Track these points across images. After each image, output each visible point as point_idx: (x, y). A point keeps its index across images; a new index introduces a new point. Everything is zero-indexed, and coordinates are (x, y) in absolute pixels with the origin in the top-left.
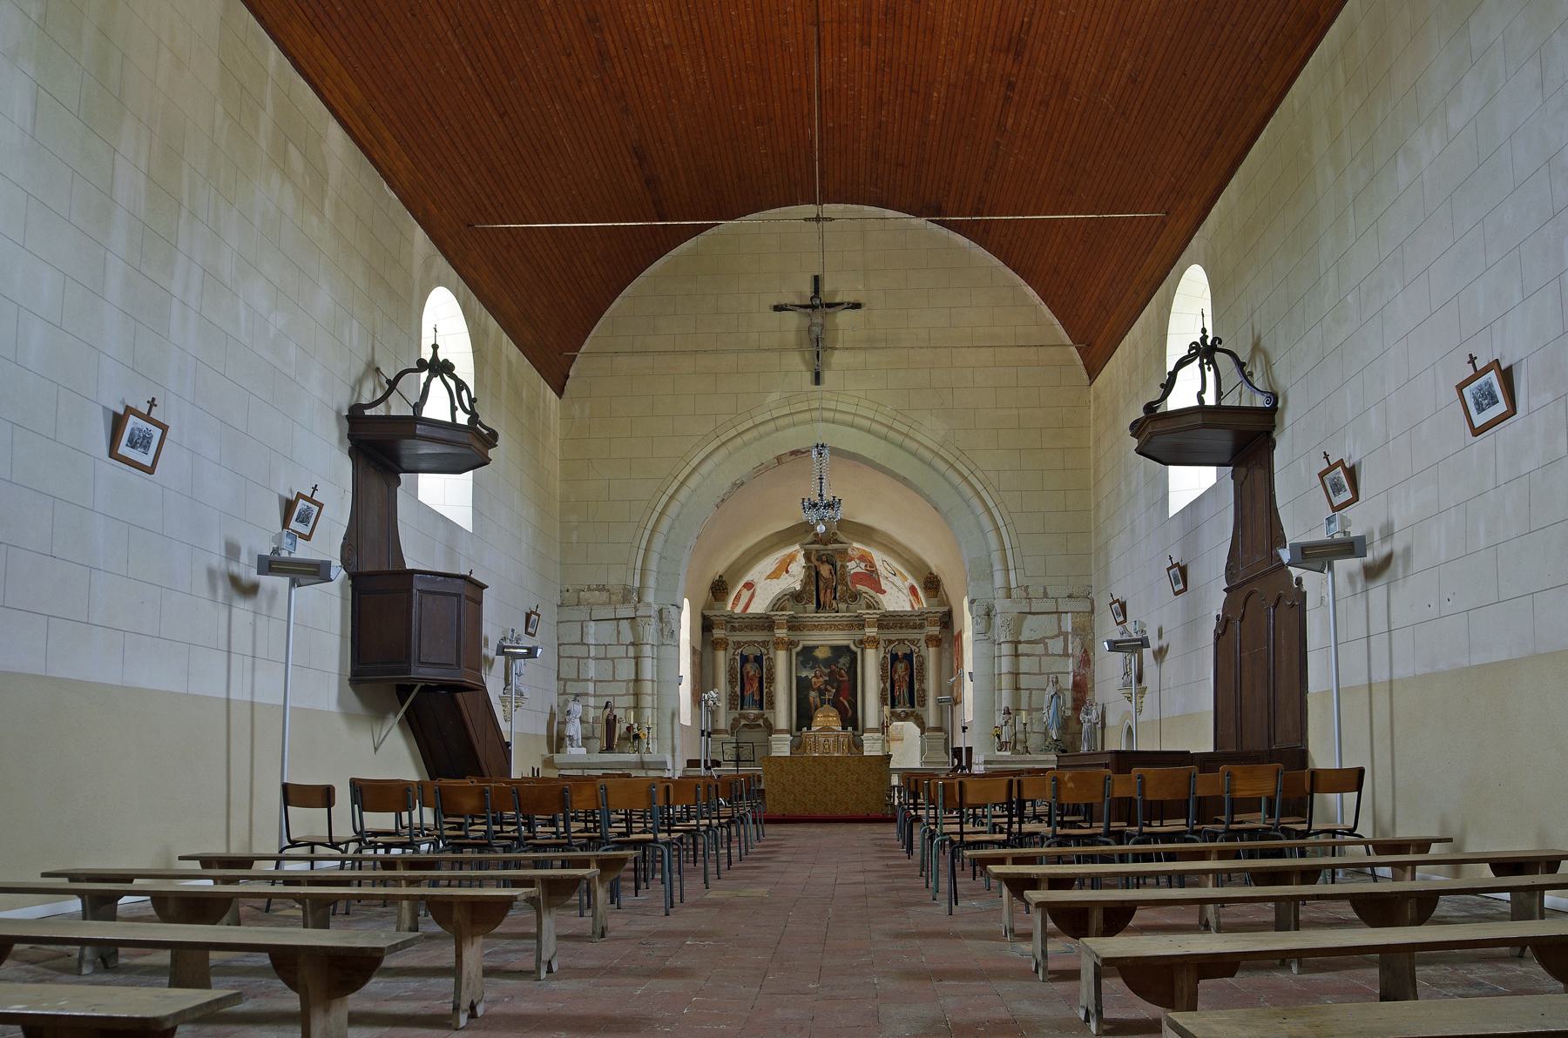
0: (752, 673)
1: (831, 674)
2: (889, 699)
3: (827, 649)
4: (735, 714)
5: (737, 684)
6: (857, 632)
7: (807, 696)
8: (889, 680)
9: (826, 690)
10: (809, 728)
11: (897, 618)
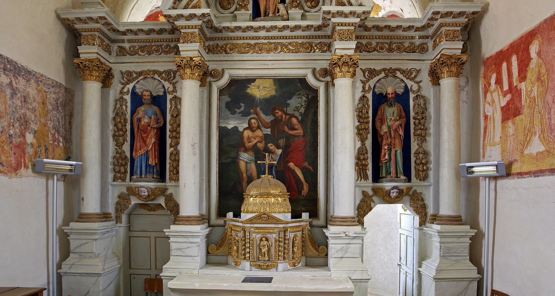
0: (145, 121)
1: (274, 124)
2: (370, 167)
3: (269, 84)
4: (121, 187)
5: (125, 140)
6: (318, 55)
7: (235, 161)
8: (370, 136)
9: (267, 150)
10: (237, 215)
11: (386, 33)
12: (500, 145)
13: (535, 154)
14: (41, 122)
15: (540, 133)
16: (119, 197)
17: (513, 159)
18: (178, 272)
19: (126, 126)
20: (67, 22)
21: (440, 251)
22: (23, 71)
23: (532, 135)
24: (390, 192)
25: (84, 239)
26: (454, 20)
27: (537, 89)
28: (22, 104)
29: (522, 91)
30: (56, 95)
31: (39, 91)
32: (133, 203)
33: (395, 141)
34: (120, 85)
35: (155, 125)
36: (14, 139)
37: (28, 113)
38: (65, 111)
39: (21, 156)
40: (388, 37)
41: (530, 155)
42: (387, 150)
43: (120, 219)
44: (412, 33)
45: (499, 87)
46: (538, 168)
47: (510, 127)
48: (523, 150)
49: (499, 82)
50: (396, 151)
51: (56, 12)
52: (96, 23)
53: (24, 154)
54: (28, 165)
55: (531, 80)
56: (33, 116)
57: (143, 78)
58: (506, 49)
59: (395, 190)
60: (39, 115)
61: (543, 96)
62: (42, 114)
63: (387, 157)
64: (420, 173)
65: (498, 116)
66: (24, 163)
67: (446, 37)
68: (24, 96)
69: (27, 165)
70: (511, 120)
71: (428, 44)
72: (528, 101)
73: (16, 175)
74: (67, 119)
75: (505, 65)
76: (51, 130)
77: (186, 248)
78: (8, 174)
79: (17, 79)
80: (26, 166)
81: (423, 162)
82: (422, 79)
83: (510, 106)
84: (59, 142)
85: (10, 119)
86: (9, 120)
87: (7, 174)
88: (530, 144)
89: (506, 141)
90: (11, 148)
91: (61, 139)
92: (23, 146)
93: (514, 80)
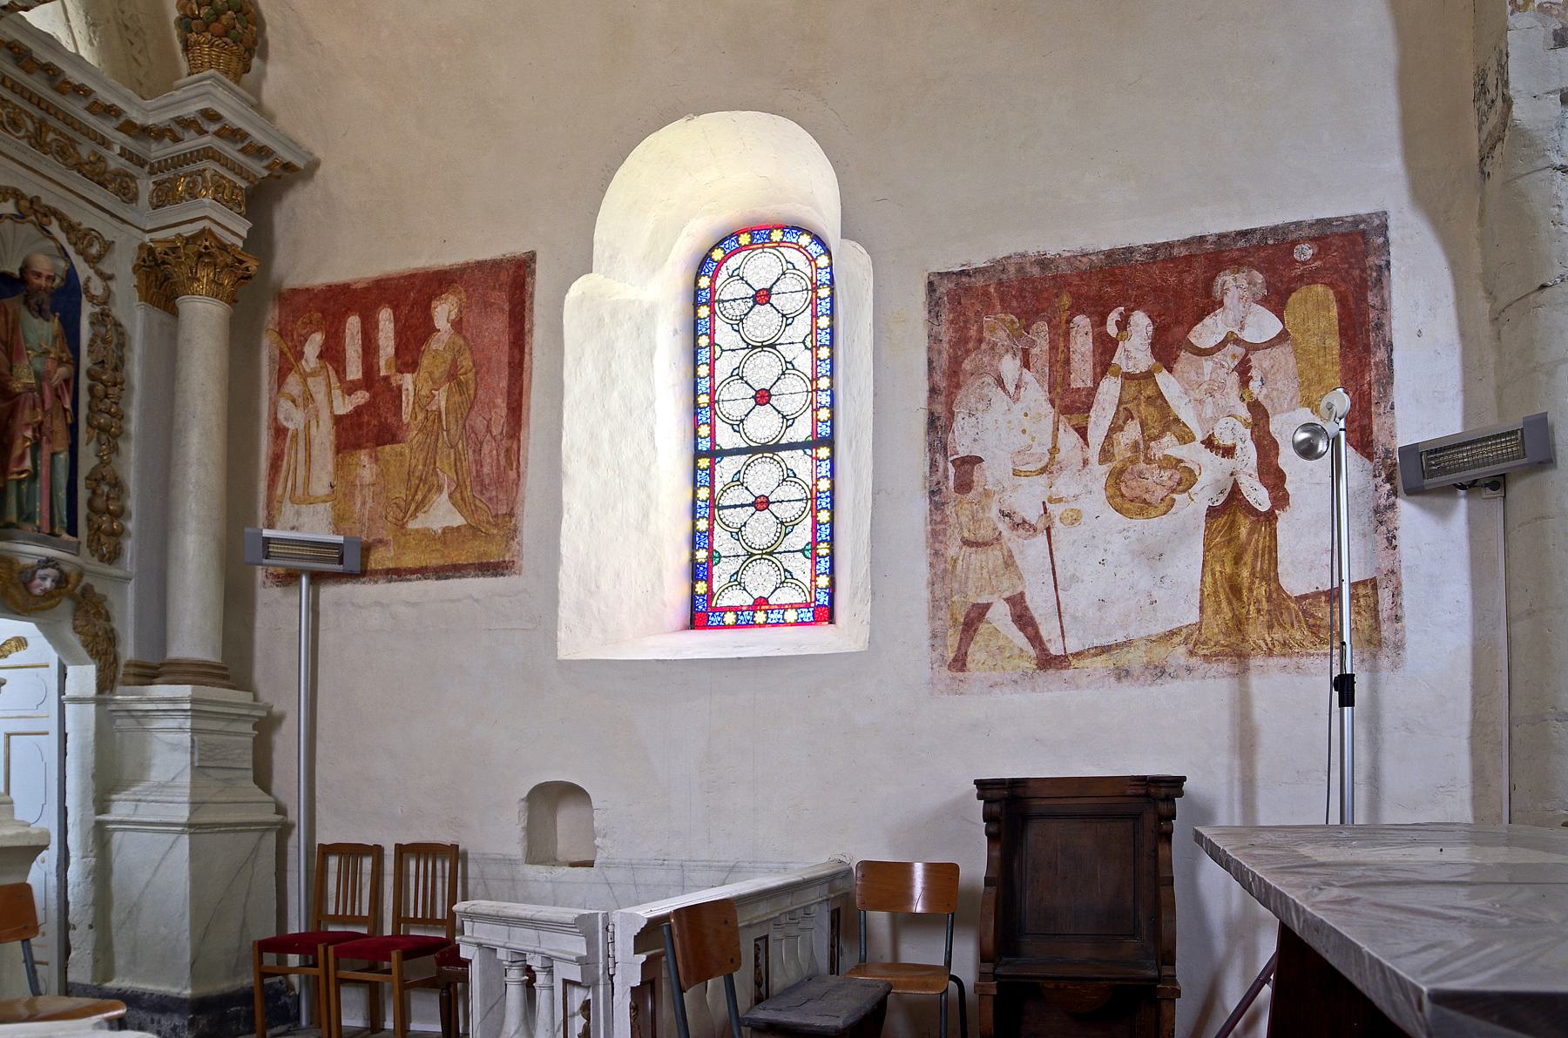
11: (37, 84)
12: (328, 504)
13: (440, 531)
15: (453, 489)
17: (373, 538)
21: (192, 753)
23: (429, 490)
24: (34, 573)
26: (241, 158)
27: (447, 396)
29: (404, 393)
33: (52, 422)
40: (39, 102)
41: (426, 534)
42: (28, 444)
44: (107, 128)
45: (330, 368)
46: (446, 562)
47: (365, 466)
48: (405, 521)
49: (332, 354)
50: (53, 455)
55: (430, 374)
58: (360, 286)
59: (49, 571)
61: (462, 414)
63: (28, 464)
64: (103, 539)
65: (324, 435)
67: (216, 191)
70: (367, 450)
71: (138, 181)
72: (421, 417)
75: (353, 323)
81: (111, 508)
82: (116, 274)
83: (366, 418)
88: (426, 509)
89: (349, 496)
93: (382, 363)
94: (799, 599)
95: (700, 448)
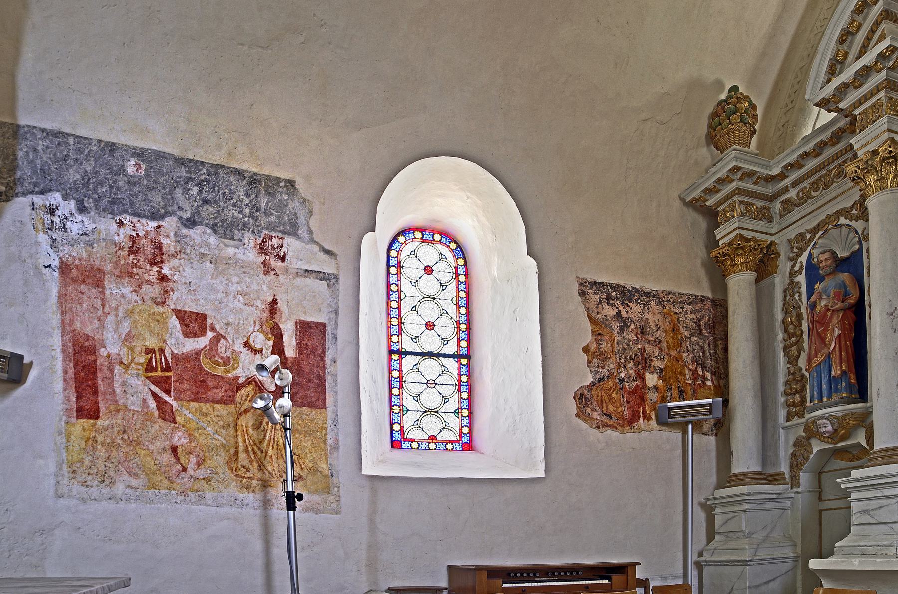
14: (669, 356)
16: (795, 445)
18: (860, 553)
19: (801, 325)
20: (698, 204)
22: (636, 294)
25: (730, 512)
28: (637, 338)
30: (697, 314)
31: (665, 315)
32: (815, 451)
34: (789, 263)
35: (837, 304)
36: (627, 384)
37: (648, 347)
38: (715, 333)
39: (638, 405)
43: (797, 480)
51: (680, 197)
52: (731, 183)
53: (644, 401)
54: (650, 415)
56: (656, 351)
57: (821, 235)
60: (667, 346)
62: (671, 345)
66: (643, 413)
68: (640, 326)
69: (647, 416)
73: (631, 429)
74: (720, 345)
76: (689, 364)
77: (876, 508)
78: (619, 427)
79: (628, 306)
80: (647, 416)
84: (705, 379)
85: (620, 359)
86: (618, 359)
87: (616, 428)
90: (622, 395)
91: (709, 375)
92: (641, 390)
94: (453, 438)
95: (392, 349)
